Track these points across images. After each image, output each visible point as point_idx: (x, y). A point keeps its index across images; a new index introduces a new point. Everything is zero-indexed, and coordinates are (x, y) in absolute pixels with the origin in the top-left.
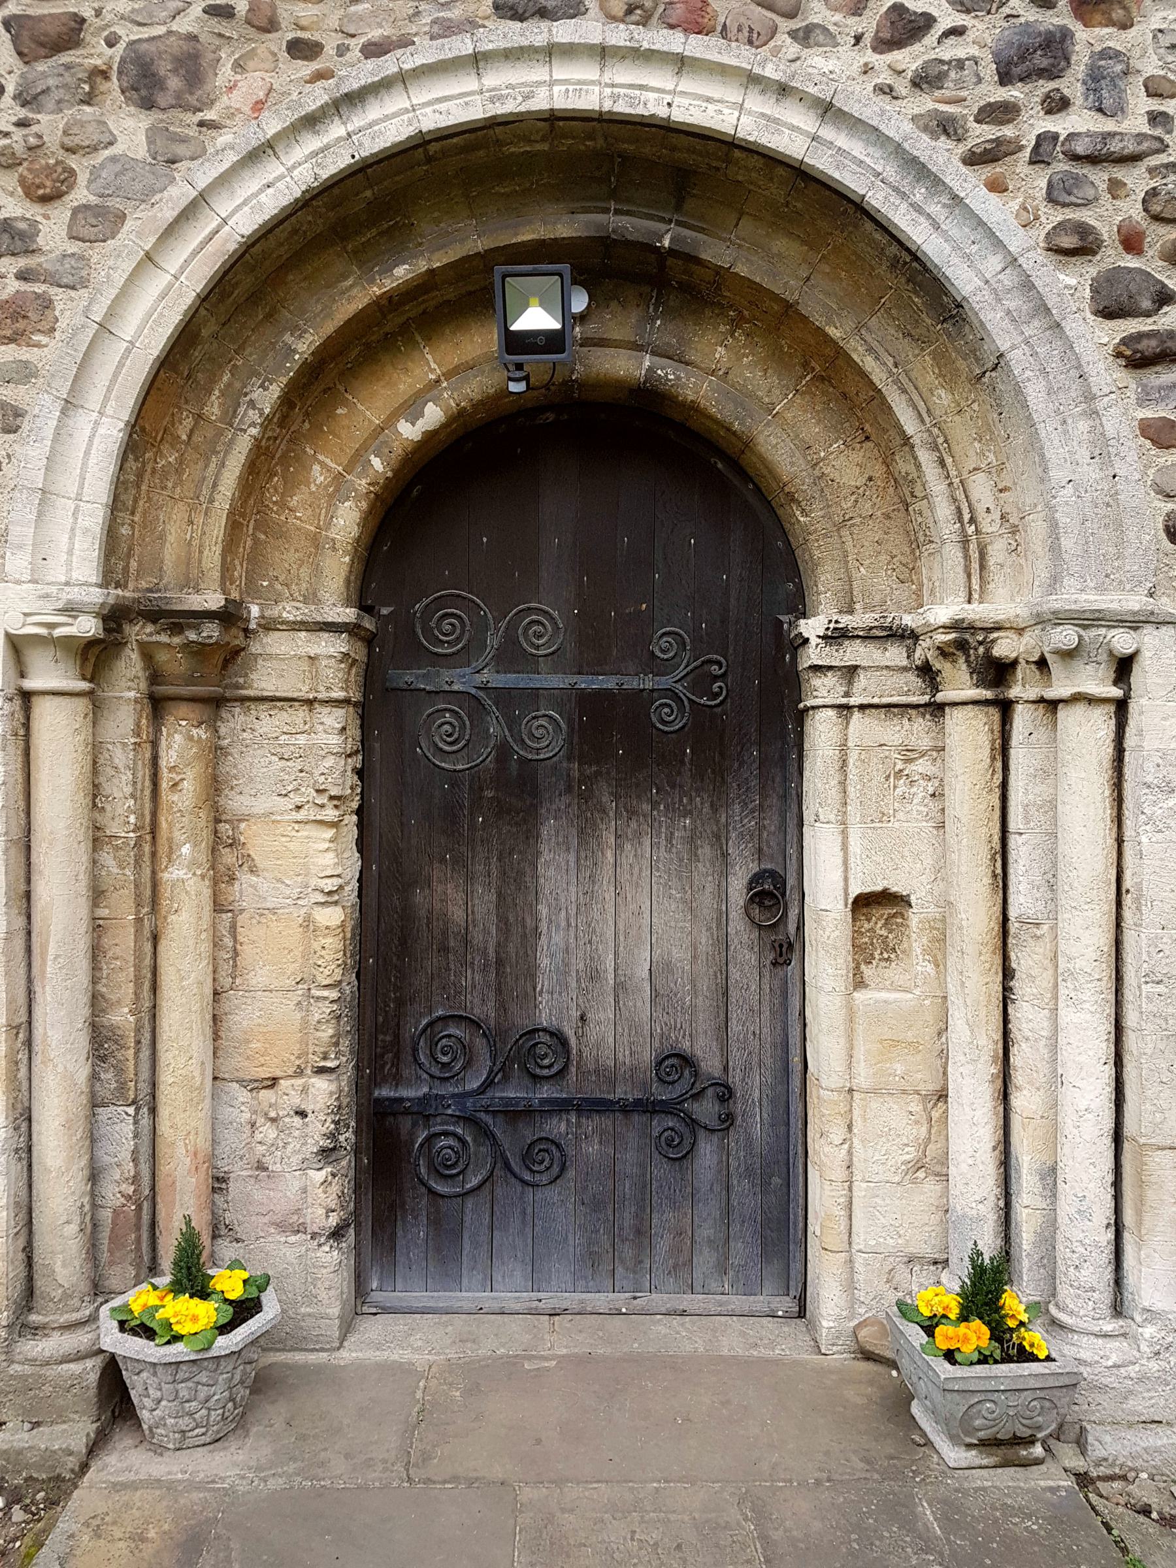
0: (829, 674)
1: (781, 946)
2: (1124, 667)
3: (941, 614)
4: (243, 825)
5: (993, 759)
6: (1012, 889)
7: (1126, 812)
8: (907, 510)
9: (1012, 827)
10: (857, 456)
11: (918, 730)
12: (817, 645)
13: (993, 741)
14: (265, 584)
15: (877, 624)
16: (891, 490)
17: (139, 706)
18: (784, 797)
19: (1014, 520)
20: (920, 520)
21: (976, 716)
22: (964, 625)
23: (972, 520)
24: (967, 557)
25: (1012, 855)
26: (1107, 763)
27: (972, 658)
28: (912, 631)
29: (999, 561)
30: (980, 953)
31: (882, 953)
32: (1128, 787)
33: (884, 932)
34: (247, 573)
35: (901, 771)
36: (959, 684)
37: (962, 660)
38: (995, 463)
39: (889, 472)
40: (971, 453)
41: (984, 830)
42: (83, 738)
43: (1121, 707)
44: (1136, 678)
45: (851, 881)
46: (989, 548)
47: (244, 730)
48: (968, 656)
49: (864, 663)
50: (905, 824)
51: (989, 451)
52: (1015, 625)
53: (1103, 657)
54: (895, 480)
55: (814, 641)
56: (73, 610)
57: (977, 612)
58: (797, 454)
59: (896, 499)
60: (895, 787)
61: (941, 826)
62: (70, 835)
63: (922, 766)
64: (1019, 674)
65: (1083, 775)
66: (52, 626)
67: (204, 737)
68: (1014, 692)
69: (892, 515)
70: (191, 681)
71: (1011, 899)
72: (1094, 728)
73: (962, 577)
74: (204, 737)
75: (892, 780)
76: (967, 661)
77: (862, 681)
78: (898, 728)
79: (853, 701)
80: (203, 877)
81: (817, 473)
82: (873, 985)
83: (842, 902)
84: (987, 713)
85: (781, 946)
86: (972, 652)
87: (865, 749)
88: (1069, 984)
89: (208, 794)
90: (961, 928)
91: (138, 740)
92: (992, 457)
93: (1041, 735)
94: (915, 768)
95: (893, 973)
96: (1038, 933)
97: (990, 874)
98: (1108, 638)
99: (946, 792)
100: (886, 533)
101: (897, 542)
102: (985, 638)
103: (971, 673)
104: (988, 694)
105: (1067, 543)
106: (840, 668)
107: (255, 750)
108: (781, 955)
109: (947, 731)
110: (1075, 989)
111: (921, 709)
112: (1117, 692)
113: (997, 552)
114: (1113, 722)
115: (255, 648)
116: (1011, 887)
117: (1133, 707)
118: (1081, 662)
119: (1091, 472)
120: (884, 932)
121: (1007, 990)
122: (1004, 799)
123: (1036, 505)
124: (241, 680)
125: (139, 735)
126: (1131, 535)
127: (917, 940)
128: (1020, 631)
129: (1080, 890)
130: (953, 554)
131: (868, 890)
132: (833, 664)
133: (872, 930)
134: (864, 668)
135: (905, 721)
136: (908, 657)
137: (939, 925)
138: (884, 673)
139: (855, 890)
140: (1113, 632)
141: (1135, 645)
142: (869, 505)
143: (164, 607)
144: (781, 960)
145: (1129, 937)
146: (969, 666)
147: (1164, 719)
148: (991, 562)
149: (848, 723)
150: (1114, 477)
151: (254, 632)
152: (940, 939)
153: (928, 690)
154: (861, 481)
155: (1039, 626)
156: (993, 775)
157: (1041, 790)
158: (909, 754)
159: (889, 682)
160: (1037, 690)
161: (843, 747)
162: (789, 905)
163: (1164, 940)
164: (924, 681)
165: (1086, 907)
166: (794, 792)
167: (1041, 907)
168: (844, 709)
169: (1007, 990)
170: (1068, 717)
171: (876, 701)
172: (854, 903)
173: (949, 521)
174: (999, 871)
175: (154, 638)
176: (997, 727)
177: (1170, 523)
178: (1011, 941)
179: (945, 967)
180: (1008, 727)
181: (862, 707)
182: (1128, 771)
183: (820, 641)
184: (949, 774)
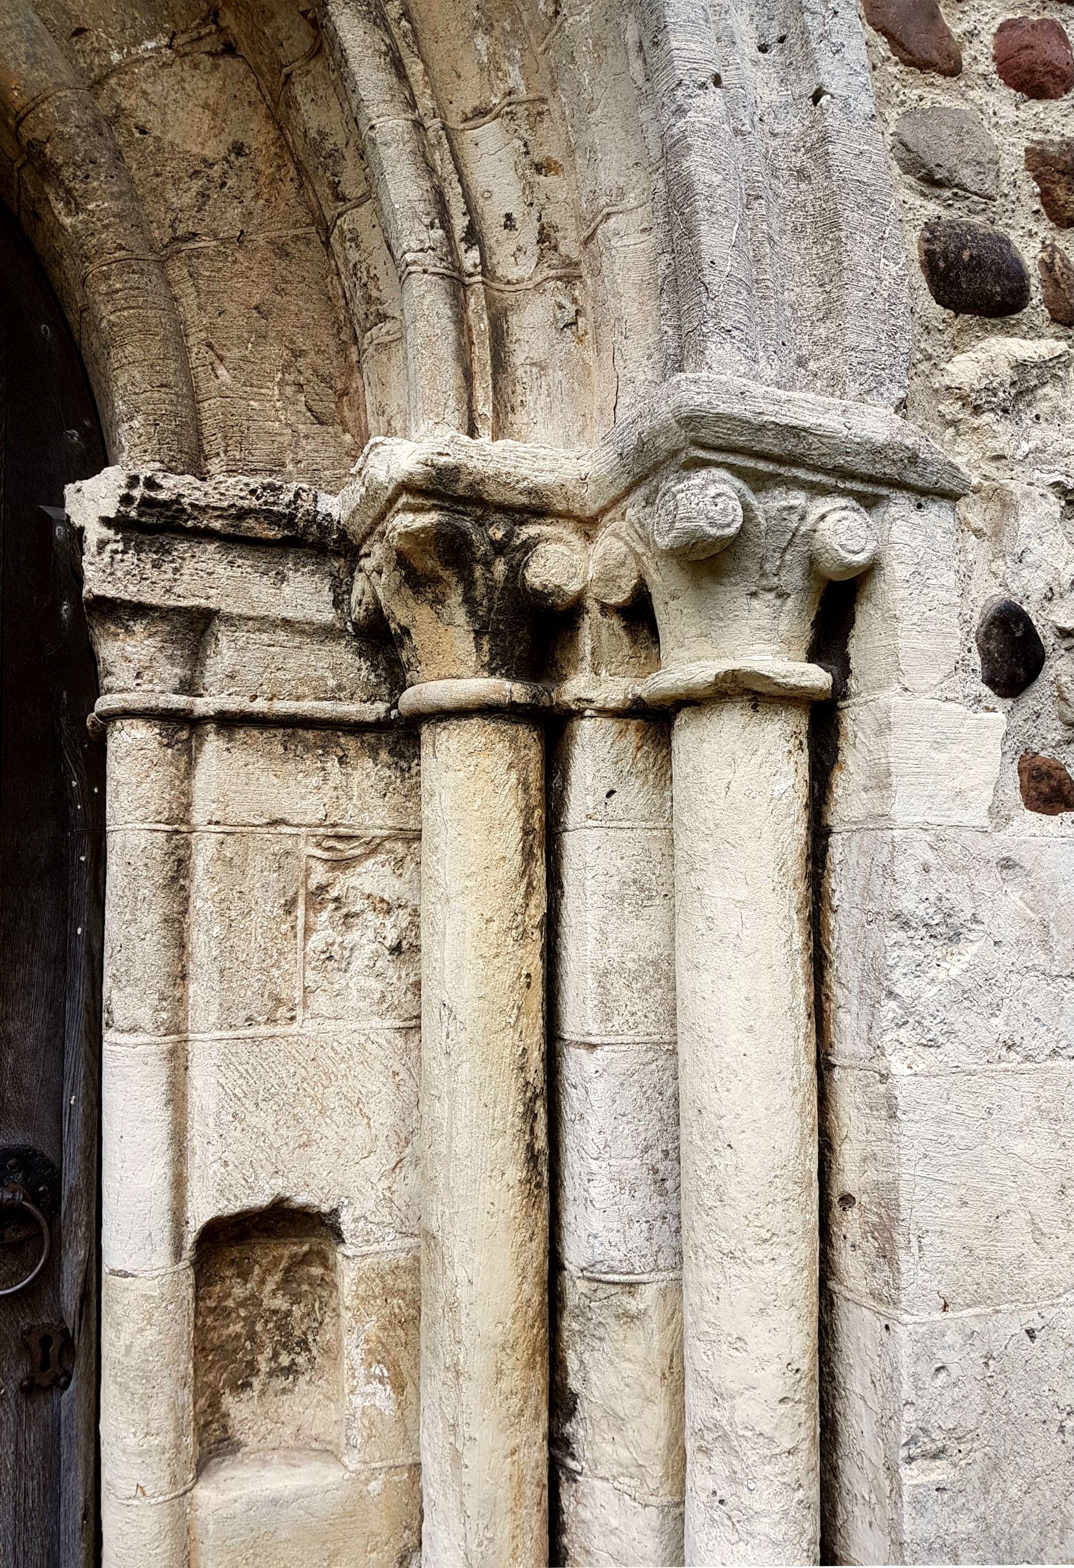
0: (138, 628)
1: (46, 1342)
2: (836, 605)
3: (397, 458)
5: (528, 856)
6: (571, 1189)
7: (837, 991)
8: (327, 244)
9: (572, 1026)
10: (205, 85)
11: (355, 790)
12: (102, 545)
13: (527, 812)
15: (255, 503)
16: (289, 189)
18: (61, 962)
19: (569, 246)
20: (354, 256)
21: (489, 747)
22: (460, 489)
23: (473, 236)
24: (461, 321)
25: (573, 1102)
26: (795, 866)
27: (480, 590)
28: (343, 534)
29: (536, 356)
30: (500, 1372)
31: (275, 1356)
32: (842, 928)
33: (280, 1303)
35: (322, 888)
36: (453, 666)
37: (455, 598)
38: (523, 94)
39: (283, 144)
40: (469, 69)
41: (510, 1038)
43: (823, 725)
44: (865, 643)
45: (194, 1187)
46: (513, 319)
48: (469, 585)
49: (228, 606)
50: (330, 1026)
51: (510, 59)
52: (575, 507)
53: (793, 578)
54: (299, 166)
55: (94, 533)
57: (488, 457)
58: (49, 42)
59: (301, 213)
60: (308, 930)
61: (412, 1027)
63: (371, 878)
64: (586, 641)
65: (742, 893)
68: (577, 686)
69: (291, 248)
71: (570, 1215)
72: (766, 770)
73: (450, 376)
75: (300, 911)
76: (469, 600)
77: (225, 653)
78: (315, 780)
79: (204, 705)
81: (104, 106)
82: (252, 1442)
83: (165, 1249)
84: (513, 740)
85: (46, 1342)
86: (478, 571)
87: (232, 831)
88: (716, 1463)
90: (453, 1307)
92: (515, 78)
93: (634, 796)
94: (353, 881)
95: (304, 1406)
96: (633, 1305)
97: (522, 1156)
98: (811, 518)
99: (424, 942)
100: (279, 292)
101: (302, 308)
102: (509, 535)
103: (478, 634)
104: (516, 691)
105: (716, 241)
106: (165, 614)
108: (45, 1364)
109: (426, 784)
110: (733, 1478)
111: (369, 738)
112: (816, 677)
113: (532, 330)
114: (804, 758)
116: (568, 1183)
117: (856, 719)
118: (742, 589)
119: (762, 84)
120: (280, 1303)
121: (558, 1444)
122: (551, 956)
123: (622, 193)
126: (858, 252)
127: (353, 1325)
128: (588, 525)
129: (744, 1205)
130: (425, 306)
131: (233, 1208)
132: (148, 598)
133: (253, 1300)
134: (229, 620)
135: (332, 765)
136: (337, 603)
137: (405, 1282)
138: (279, 644)
139: (201, 1211)
140: (823, 505)
141: (871, 546)
142: (234, 213)
144: (44, 1379)
145: (857, 1325)
146: (472, 613)
147: (938, 745)
148: (519, 357)
149: (191, 764)
150: (816, 97)
152: (407, 1311)
153: (384, 690)
154: (214, 149)
155: (642, 492)
156: (527, 895)
157: (640, 934)
158: (342, 847)
159: (291, 663)
160: (625, 682)
161: (178, 827)
162: (66, 1239)
163: (949, 1339)
164: (374, 667)
165: (759, 1253)
166: (81, 949)
167: (640, 1242)
168: (181, 727)
169: (558, 1444)
170: (700, 742)
171: (260, 706)
172: (199, 1243)
173: (416, 216)
174: (541, 1143)
176: (534, 777)
177: (937, 247)
178: (569, 1324)
179: (417, 1389)
180: (557, 782)
181: (229, 722)
182: (841, 888)
183: (110, 533)
184: (430, 895)
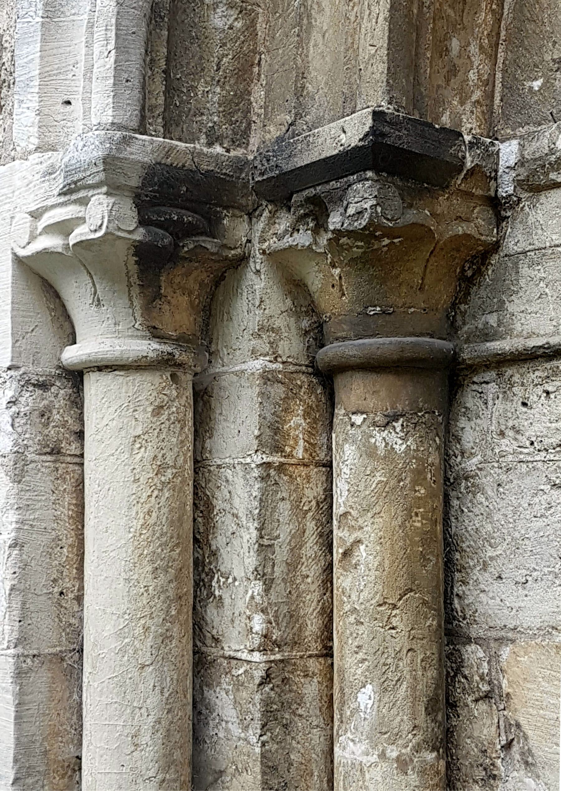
4: (506, 652)
14: (537, 85)
17: (278, 391)
34: (504, 71)
42: (148, 454)
47: (502, 434)
56: (77, 190)
62: (122, 651)
66: (63, 228)
67: (400, 447)
70: (364, 327)
74: (400, 447)
80: (402, 764)
89: (412, 577)
91: (276, 459)
107: (522, 477)
115: (515, 240)
124: (492, 320)
125: (277, 449)
143: (287, 167)
151: (513, 203)
175: (288, 241)
